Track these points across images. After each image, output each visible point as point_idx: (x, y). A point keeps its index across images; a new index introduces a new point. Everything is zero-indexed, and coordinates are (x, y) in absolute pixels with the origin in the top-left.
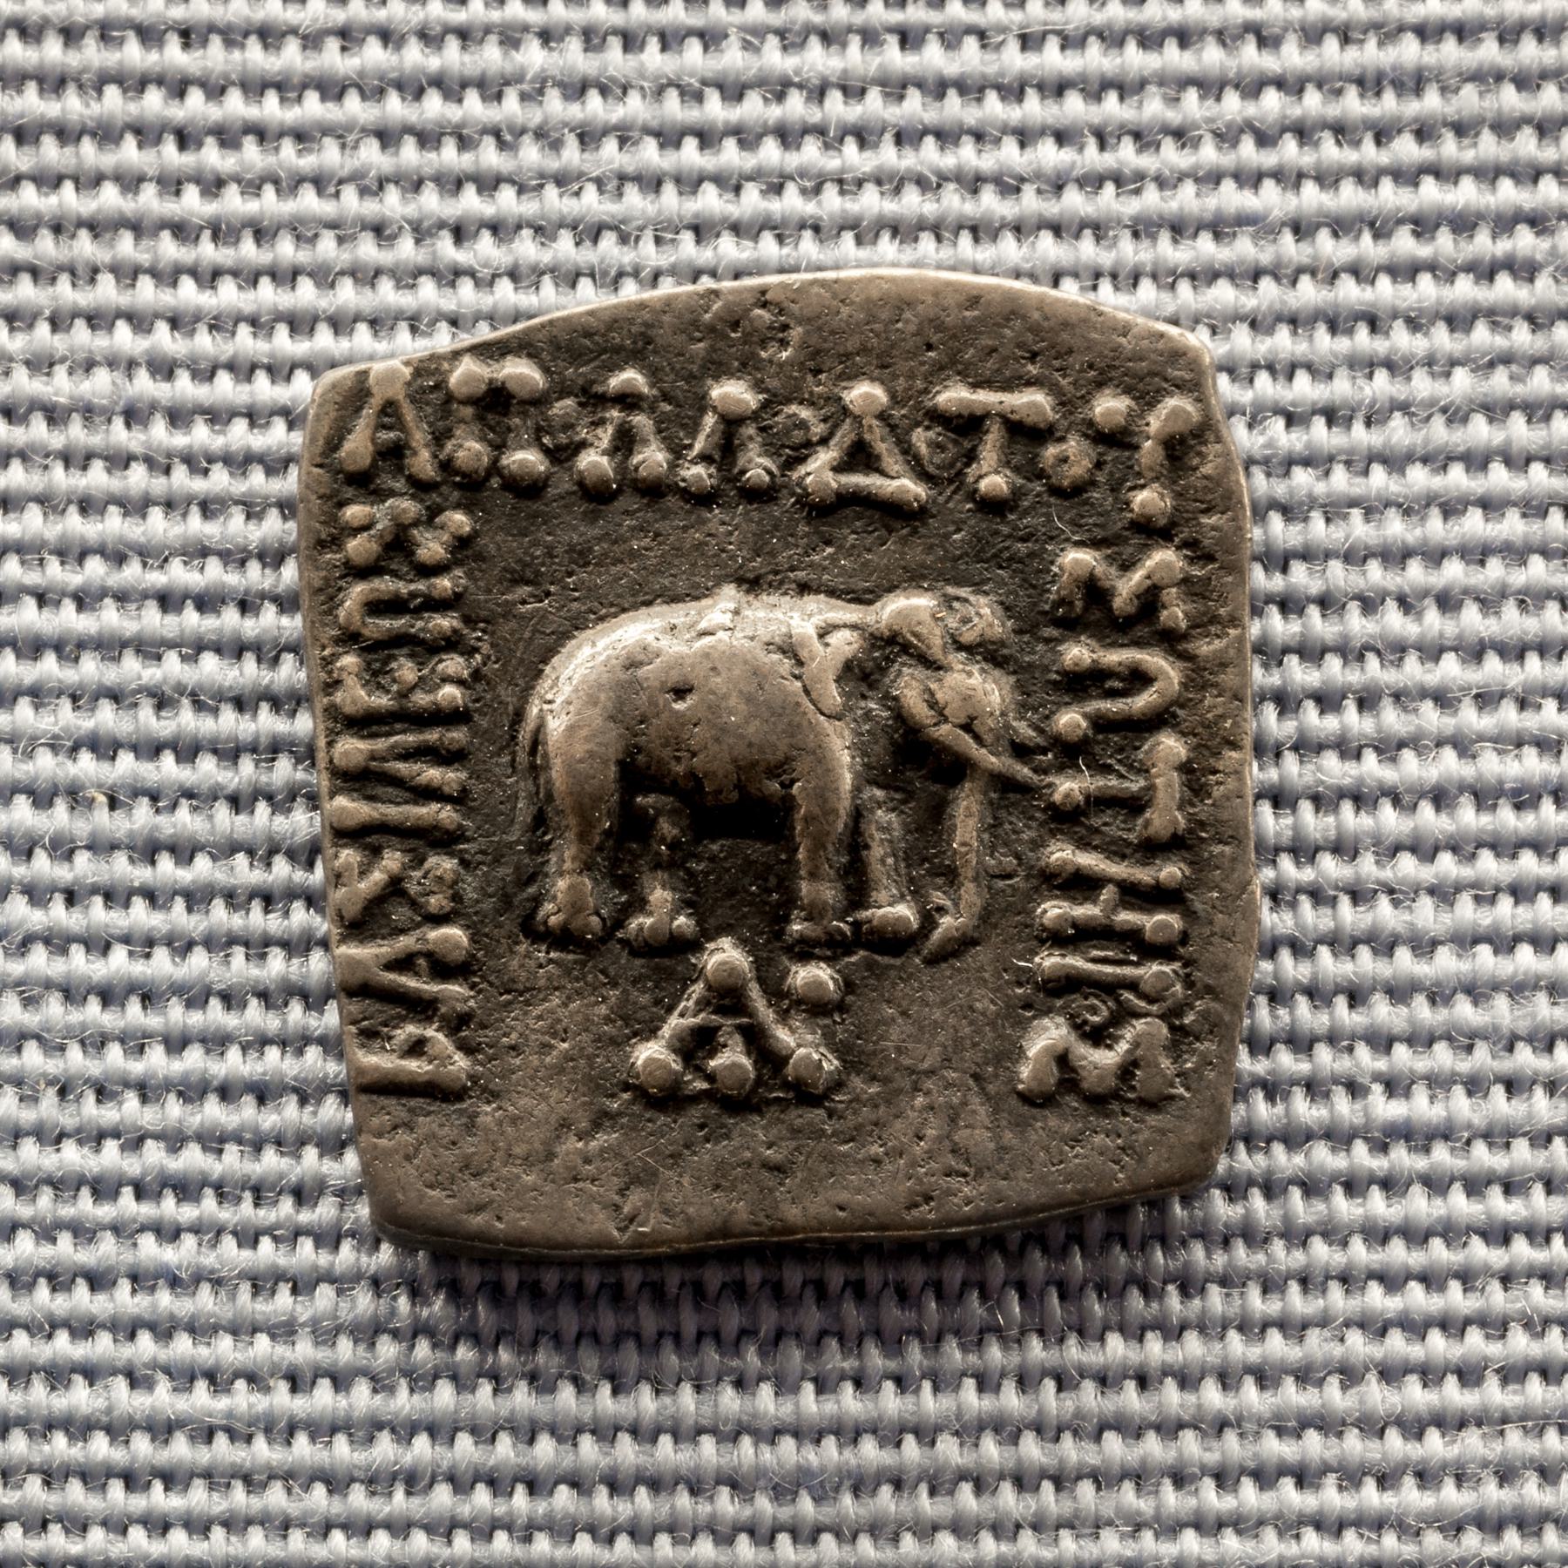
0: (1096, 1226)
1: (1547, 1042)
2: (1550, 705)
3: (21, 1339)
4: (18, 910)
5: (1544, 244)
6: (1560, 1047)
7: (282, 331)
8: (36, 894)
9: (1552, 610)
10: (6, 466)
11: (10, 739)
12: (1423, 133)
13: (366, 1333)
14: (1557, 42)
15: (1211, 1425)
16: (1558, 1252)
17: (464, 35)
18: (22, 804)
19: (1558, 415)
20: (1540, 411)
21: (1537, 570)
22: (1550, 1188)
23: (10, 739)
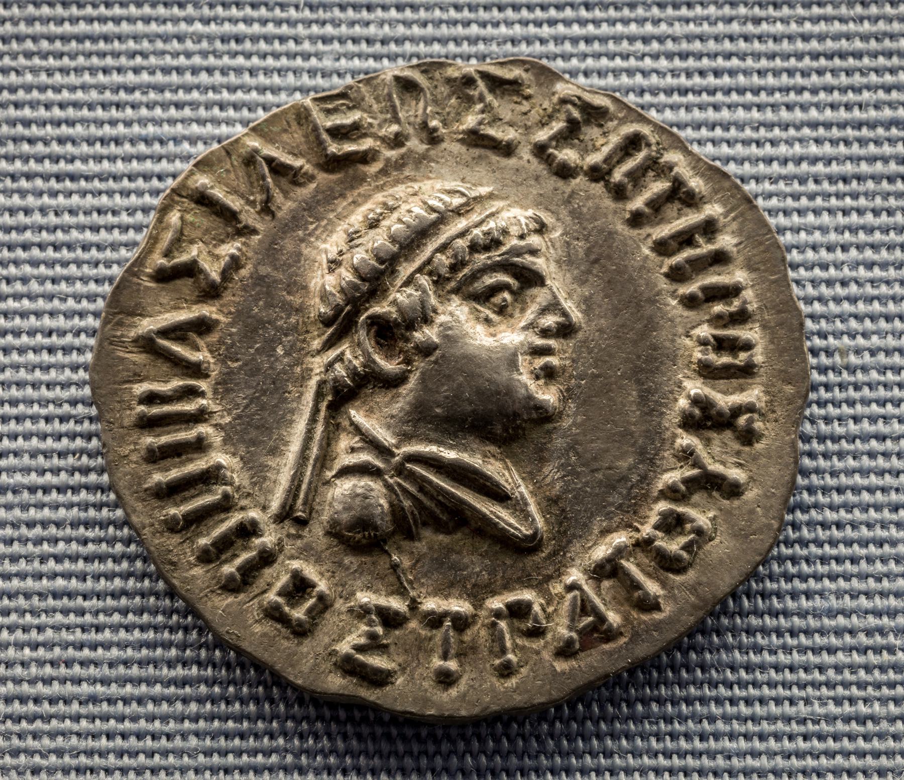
18: (7, 216)
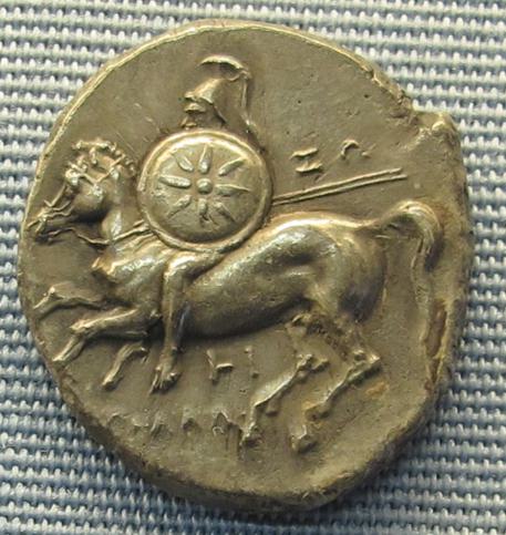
0: (317, 517)
1: (500, 122)
2: (500, 106)
3: (8, 29)
4: (9, 31)
5: (497, 349)
6: (503, 208)
7: (69, 47)
8: (12, 483)
9: (501, 24)
10: (3, 213)
11: (4, 89)
12: (439, 69)
13: (92, 472)
14: (501, 481)
15: (365, 45)
16: (504, 518)
17: (120, 13)
18: (7, 214)
19: (503, 343)
20: (497, 477)
21: (494, 93)
22: (501, 139)
23: (4, 89)
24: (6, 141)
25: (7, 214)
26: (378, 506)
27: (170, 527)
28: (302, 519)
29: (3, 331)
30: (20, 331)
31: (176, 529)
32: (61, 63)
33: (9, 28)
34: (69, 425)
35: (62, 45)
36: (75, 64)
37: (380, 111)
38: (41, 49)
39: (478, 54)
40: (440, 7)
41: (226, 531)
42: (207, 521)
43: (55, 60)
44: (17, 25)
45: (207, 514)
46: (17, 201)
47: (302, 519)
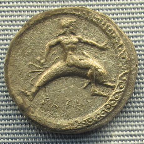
8: (3, 106)
18: (2, 140)
24: (2, 134)
25: (2, 140)
26: (101, 132)
27: (75, 142)
28: (76, 137)
29: (1, 92)
30: (4, 111)
31: (76, 142)
32: (17, 7)
33: (2, 130)
34: (20, 116)
35: (16, 12)
36: (21, 7)
37: (24, 116)
38: (11, 13)
39: (117, 14)
40: (109, 2)
41: (50, 142)
42: (61, 140)
43: (14, 16)
44: (4, 129)
45: (53, 138)
46: (5, 51)
47: (76, 137)
